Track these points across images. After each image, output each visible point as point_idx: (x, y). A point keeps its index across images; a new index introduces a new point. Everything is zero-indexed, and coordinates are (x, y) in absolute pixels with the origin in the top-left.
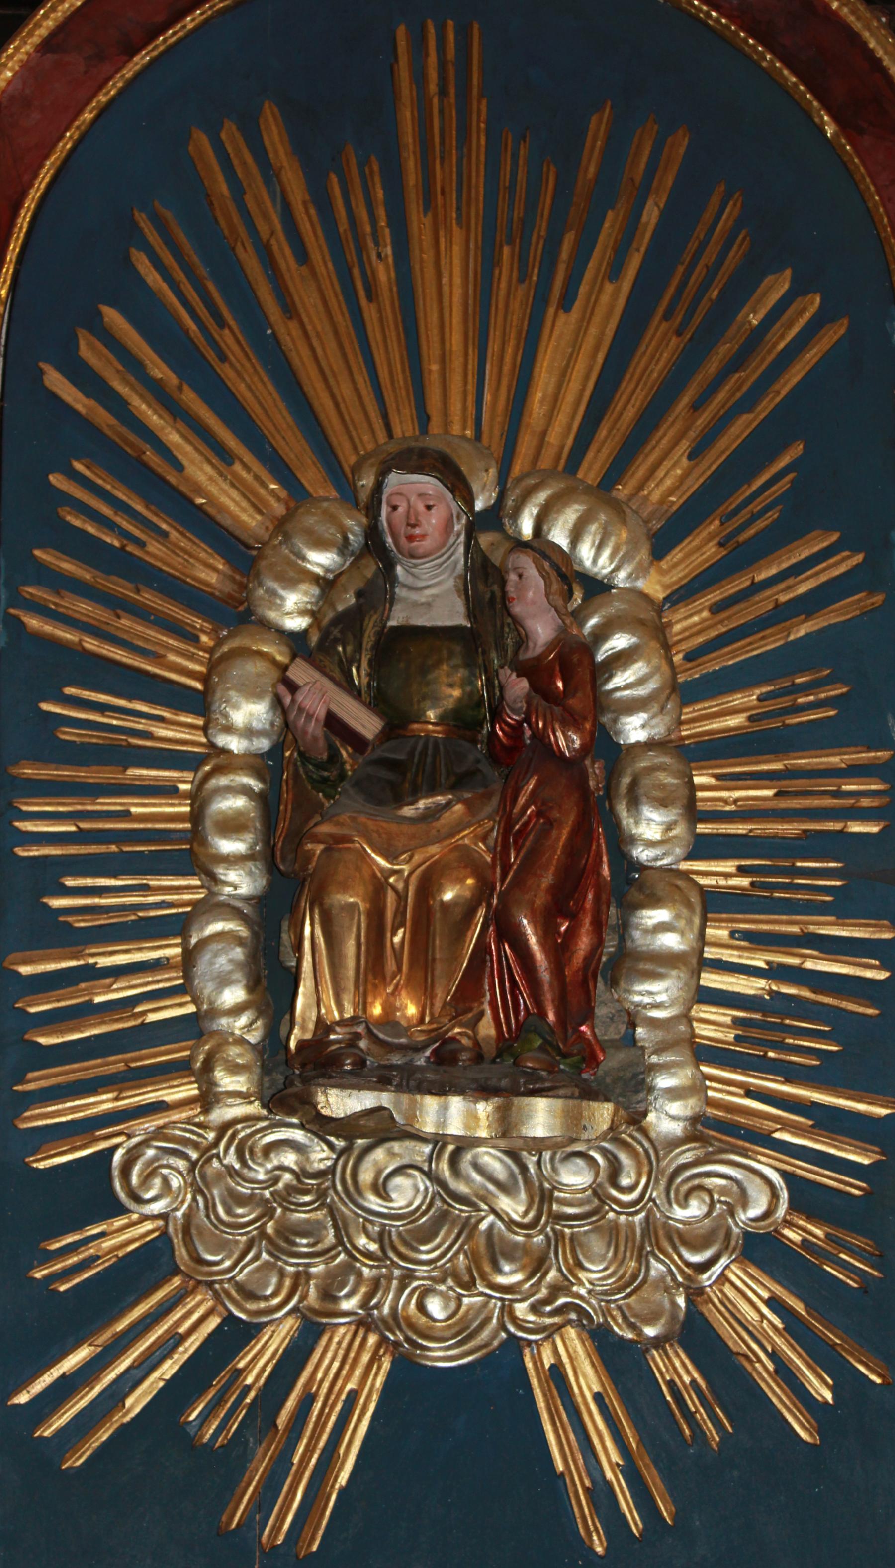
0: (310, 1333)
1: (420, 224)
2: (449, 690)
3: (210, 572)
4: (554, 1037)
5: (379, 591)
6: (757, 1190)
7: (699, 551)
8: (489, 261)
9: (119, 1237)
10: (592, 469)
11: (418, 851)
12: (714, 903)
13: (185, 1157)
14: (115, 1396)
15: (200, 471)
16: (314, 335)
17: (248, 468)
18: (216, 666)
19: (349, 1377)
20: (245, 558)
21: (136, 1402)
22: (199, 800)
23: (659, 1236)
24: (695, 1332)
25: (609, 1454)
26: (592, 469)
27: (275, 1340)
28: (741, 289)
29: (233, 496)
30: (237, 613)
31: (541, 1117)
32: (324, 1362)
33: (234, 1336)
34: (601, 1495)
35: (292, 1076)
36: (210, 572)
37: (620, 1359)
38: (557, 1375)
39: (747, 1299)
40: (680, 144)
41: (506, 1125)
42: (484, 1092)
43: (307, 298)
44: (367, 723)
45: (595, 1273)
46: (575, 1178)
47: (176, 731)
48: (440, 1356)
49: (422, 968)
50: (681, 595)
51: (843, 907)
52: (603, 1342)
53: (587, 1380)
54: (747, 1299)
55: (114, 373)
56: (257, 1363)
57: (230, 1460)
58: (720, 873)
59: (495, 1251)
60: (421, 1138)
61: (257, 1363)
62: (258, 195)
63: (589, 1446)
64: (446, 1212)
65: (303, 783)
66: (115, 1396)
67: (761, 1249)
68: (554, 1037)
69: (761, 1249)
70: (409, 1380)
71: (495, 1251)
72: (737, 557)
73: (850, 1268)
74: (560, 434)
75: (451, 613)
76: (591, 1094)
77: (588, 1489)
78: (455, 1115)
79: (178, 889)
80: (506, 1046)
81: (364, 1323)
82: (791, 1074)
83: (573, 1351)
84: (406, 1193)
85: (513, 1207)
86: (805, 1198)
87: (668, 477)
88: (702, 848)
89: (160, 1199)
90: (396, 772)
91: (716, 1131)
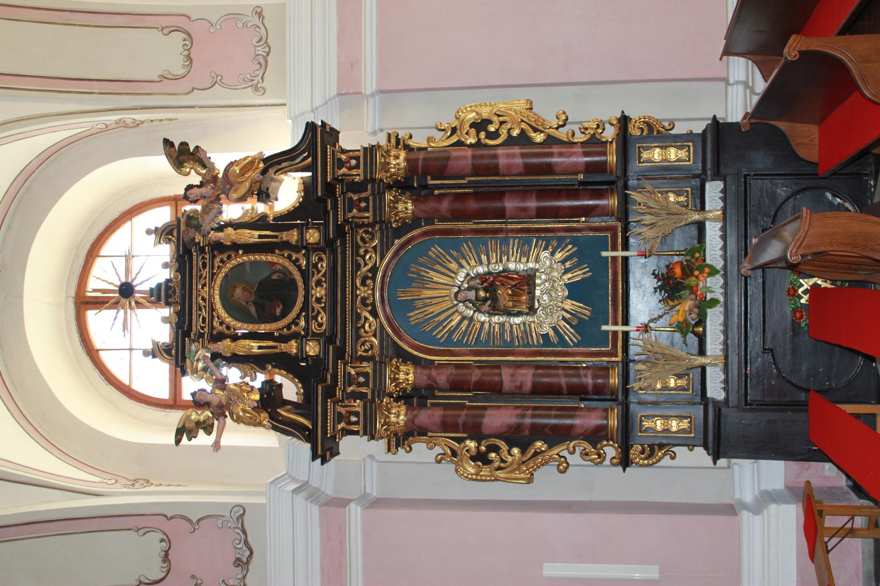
0: (563, 309)
1: (422, 296)
2: (482, 294)
3: (466, 322)
4: (528, 280)
5: (470, 301)
6: (545, 254)
7: (464, 263)
8: (427, 288)
9: (551, 333)
10: (454, 275)
11: (504, 294)
12: (508, 260)
13: (543, 323)
14: (571, 333)
15: (454, 323)
16: (436, 309)
17: (453, 317)
18: (479, 321)
19: (569, 305)
20: (464, 318)
21: (572, 331)
22: (496, 323)
23: (551, 267)
24: (563, 262)
25: (579, 272)
26: (454, 275)
27: (565, 314)
28: (430, 257)
29: (457, 319)
30: (471, 319)
31: (538, 281)
32: (567, 307)
33: (564, 319)
34: (584, 273)
35: (532, 311)
36: (466, 322)
37: (566, 271)
38: (569, 279)
39: (559, 256)
40: (412, 265)
41: (539, 285)
42: (535, 288)
43: (431, 310)
44: (489, 302)
45: (555, 274)
46: (543, 277)
47: (487, 326)
48: (567, 293)
49: (520, 295)
50: (469, 264)
51: (509, 245)
52: (564, 274)
53: (570, 275)
54: (559, 256)
55: (441, 334)
56: (568, 316)
57: (580, 319)
58: (504, 259)
59: (553, 286)
60: (377, 461)
61: (568, 316)
62: (419, 316)
63: (578, 275)
64: (548, 292)
65: (495, 310)
66: (571, 333)
67: (552, 254)
68: (528, 280)
69: (552, 254)
70: (569, 297)
71: (553, 286)
72: (464, 258)
73: (555, 243)
74: (449, 279)
75: (473, 292)
76: (535, 275)
77: (326, 182)
78: (538, 293)
79: (507, 325)
80: (528, 285)
81: (562, 302)
82: (530, 250)
83: (566, 277)
84: (545, 297)
85: (547, 284)
86: (546, 249)
87: (454, 266)
88: (501, 261)
89: (546, 329)
90: (494, 299)
91: (537, 260)
